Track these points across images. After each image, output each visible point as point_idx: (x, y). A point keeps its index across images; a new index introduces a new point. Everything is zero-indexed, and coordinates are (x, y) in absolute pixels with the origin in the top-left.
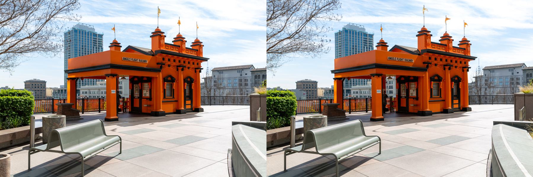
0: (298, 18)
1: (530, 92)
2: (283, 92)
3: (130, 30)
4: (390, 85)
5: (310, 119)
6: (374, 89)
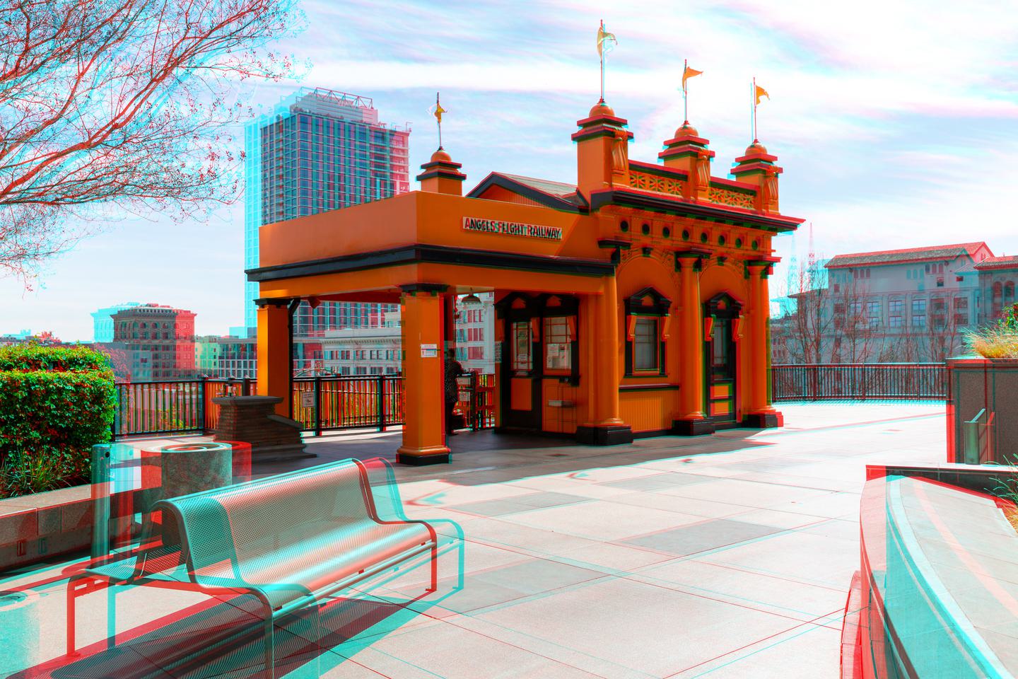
0: (119, 71)
1: (1008, 352)
2: (62, 354)
3: (501, 116)
4: (472, 326)
5: (165, 456)
6: (409, 343)
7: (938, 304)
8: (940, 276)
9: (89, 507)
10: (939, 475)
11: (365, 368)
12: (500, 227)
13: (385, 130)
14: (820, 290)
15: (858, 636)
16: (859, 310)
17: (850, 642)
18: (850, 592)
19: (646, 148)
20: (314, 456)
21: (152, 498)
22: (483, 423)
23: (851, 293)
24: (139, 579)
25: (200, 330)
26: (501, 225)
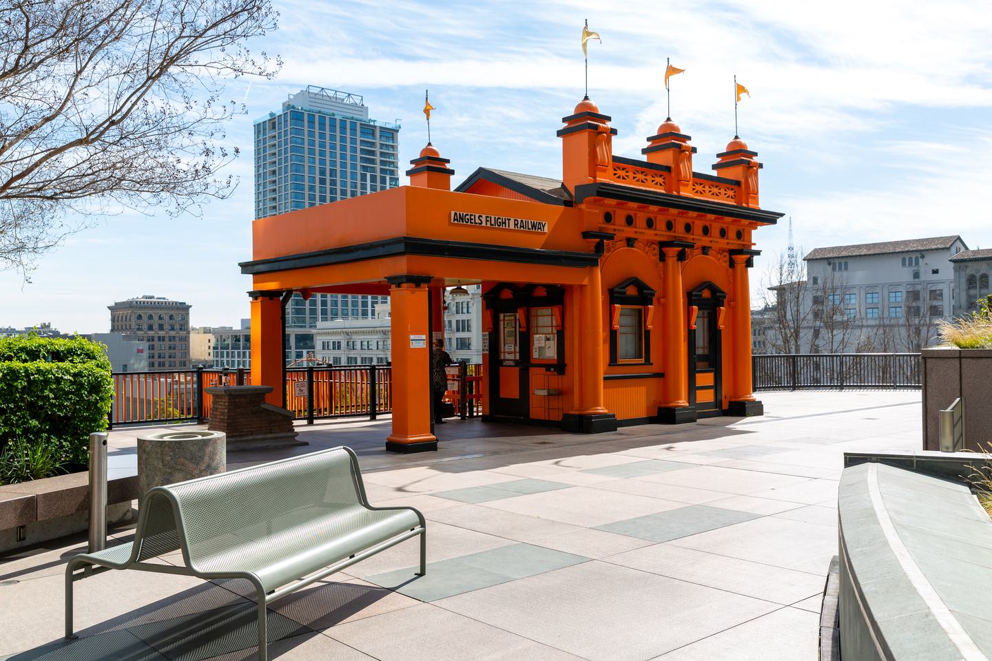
3: (489, 113)
7: (915, 295)
8: (916, 268)
9: (86, 495)
10: (915, 461)
11: (356, 358)
12: (487, 221)
13: (375, 127)
15: (836, 619)
19: (629, 144)
20: (307, 444)
21: (148, 485)
22: (471, 412)
24: (134, 563)
25: (195, 321)
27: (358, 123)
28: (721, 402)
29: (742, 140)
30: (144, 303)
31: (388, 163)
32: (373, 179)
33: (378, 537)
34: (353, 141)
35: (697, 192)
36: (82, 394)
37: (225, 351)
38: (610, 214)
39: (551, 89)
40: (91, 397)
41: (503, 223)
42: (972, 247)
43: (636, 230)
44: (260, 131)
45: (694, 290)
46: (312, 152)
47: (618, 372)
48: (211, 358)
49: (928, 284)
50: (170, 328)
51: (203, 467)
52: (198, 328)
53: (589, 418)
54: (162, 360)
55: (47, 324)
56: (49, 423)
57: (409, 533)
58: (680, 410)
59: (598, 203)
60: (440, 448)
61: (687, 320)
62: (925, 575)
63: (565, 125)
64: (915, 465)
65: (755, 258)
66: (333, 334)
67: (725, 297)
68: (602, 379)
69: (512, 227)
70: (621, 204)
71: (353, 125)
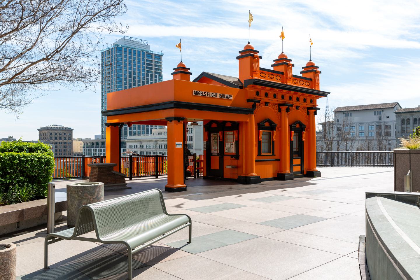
3: (205, 47)
7: (379, 127)
9: (45, 209)
10: (395, 196)
11: (144, 152)
12: (208, 94)
13: (153, 54)
14: (333, 121)
15: (365, 261)
16: (349, 130)
17: (363, 264)
18: (359, 243)
19: (266, 63)
20: (130, 188)
21: (72, 205)
22: (198, 175)
23: (345, 122)
24: (74, 237)
25: (75, 136)
26: (208, 94)
27: (146, 52)
28: (303, 171)
29: (313, 62)
30: (53, 128)
31: (158, 69)
32: (152, 76)
33: (175, 226)
34: (143, 60)
35: (294, 83)
36: (42, 166)
37: (88, 149)
38: (267, 93)
39: (227, 39)
40: (45, 168)
41: (214, 95)
42: (403, 107)
43: (269, 99)
44: (104, 55)
45: (293, 124)
46: (125, 64)
47: (261, 158)
48: (82, 151)
49: (385, 122)
50: (64, 138)
51: (95, 197)
52: (76, 138)
53: (249, 177)
54: (60, 152)
55: (11, 137)
56: (28, 178)
57: (185, 225)
58: (287, 175)
59: (254, 87)
60: (188, 190)
61: (290, 138)
62: (414, 242)
63: (240, 54)
64: (395, 198)
65: (318, 111)
66: (134, 141)
67: (305, 127)
68: (255, 161)
69: (218, 97)
70: (272, 89)
71: (143, 53)
